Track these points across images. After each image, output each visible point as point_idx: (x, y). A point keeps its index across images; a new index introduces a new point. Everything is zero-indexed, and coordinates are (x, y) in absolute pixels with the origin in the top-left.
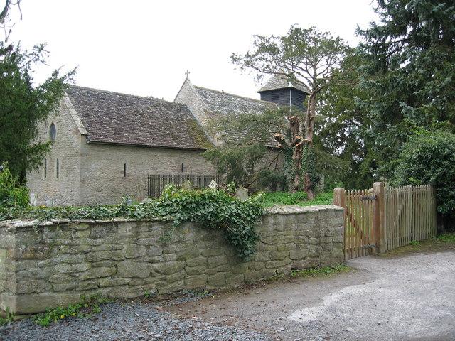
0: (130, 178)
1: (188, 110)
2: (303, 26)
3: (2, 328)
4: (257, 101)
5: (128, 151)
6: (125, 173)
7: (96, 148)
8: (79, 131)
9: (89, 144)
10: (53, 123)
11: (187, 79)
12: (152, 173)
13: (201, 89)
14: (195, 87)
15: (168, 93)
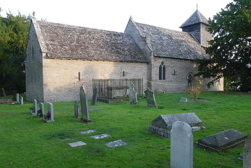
14: (137, 23)
15: (121, 28)
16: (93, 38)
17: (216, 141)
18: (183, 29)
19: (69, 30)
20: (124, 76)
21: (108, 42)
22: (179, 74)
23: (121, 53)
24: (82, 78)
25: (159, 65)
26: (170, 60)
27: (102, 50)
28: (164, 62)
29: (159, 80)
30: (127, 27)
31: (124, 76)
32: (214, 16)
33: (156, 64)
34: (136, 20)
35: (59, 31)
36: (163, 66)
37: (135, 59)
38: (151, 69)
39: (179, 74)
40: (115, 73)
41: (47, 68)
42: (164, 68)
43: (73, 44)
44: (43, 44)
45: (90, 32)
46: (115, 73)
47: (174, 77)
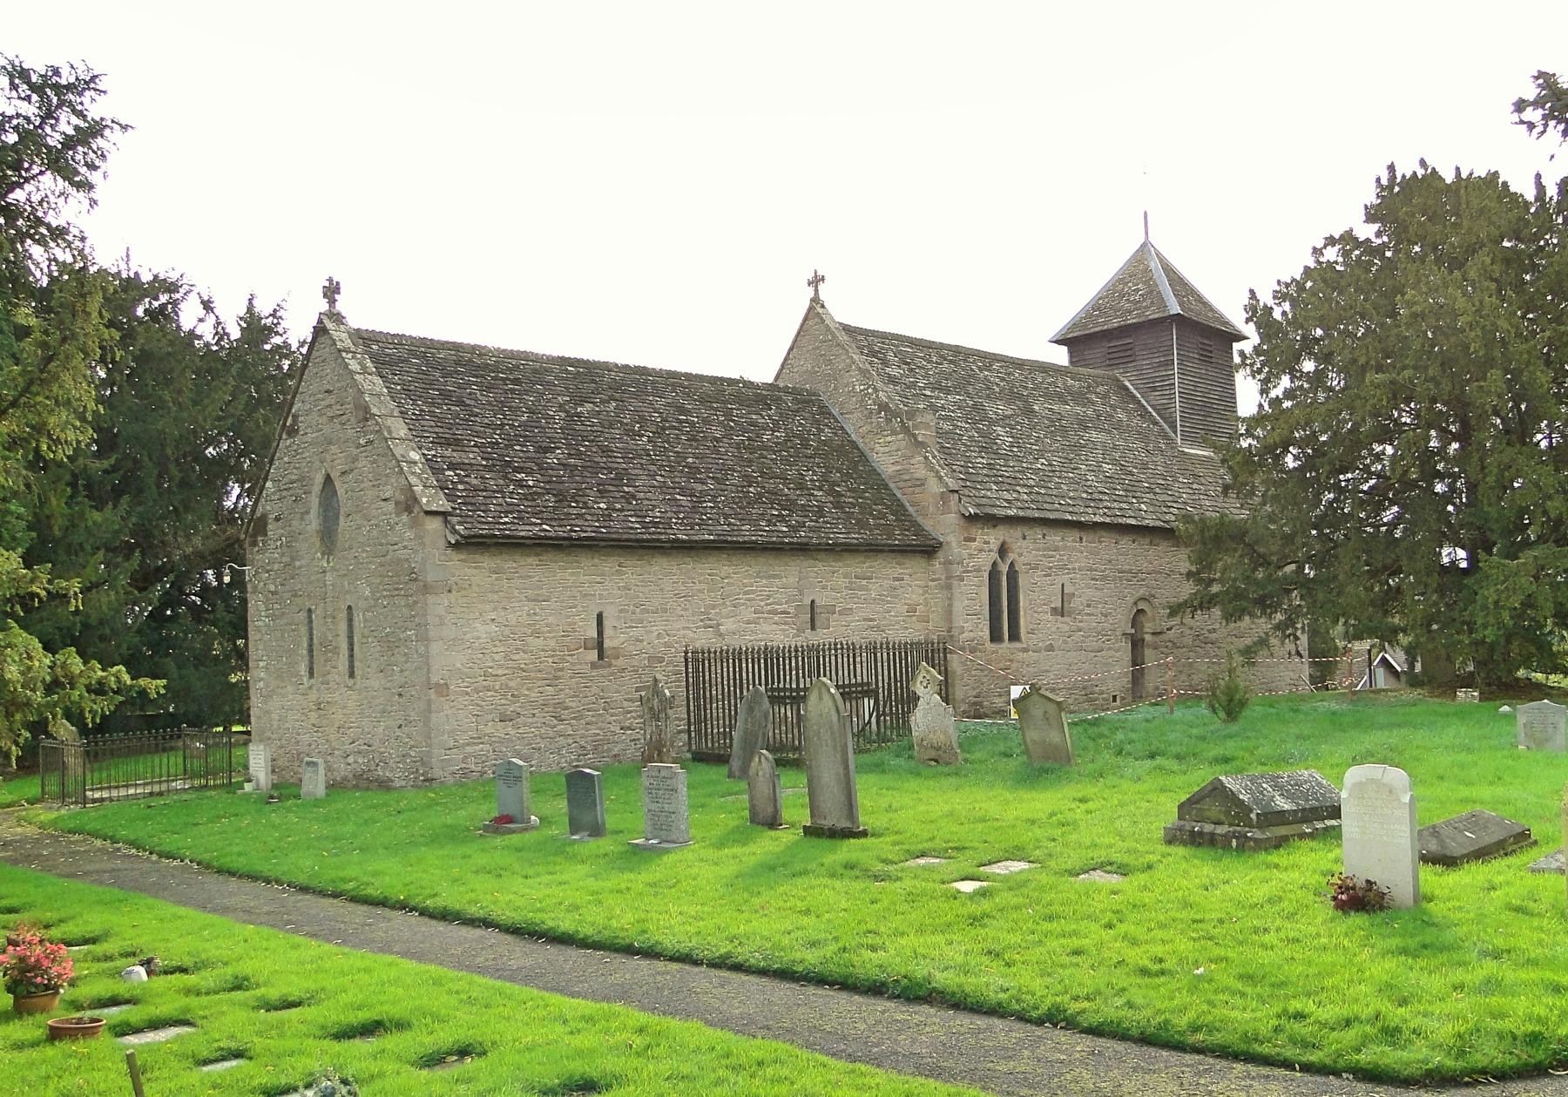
0: (620, 662)
1: (825, 412)
2: (1371, 198)
3: (1563, 328)
4: (1046, 368)
5: (609, 564)
6: (600, 645)
7: (488, 562)
8: (416, 500)
9: (456, 546)
10: (328, 479)
11: (816, 300)
12: (704, 640)
13: (867, 333)
14: (847, 329)
15: (754, 354)
16: (642, 420)
17: (1442, 843)
18: (1070, 352)
19: (516, 381)
20: (813, 628)
21: (716, 439)
22: (1087, 610)
23: (794, 503)
24: (615, 643)
25: (986, 560)
26: (1038, 532)
27: (699, 487)
28: (1014, 547)
29: (988, 645)
30: (791, 349)
31: (813, 628)
32: (1279, 282)
33: (974, 553)
34: (844, 309)
35: (469, 384)
36: (1004, 569)
37: (866, 535)
38: (949, 587)
39: (1087, 610)
40: (769, 612)
41: (445, 599)
42: (1013, 575)
43: (551, 459)
44: (415, 463)
45: (616, 387)
46: (769, 612)
47: (1064, 624)
